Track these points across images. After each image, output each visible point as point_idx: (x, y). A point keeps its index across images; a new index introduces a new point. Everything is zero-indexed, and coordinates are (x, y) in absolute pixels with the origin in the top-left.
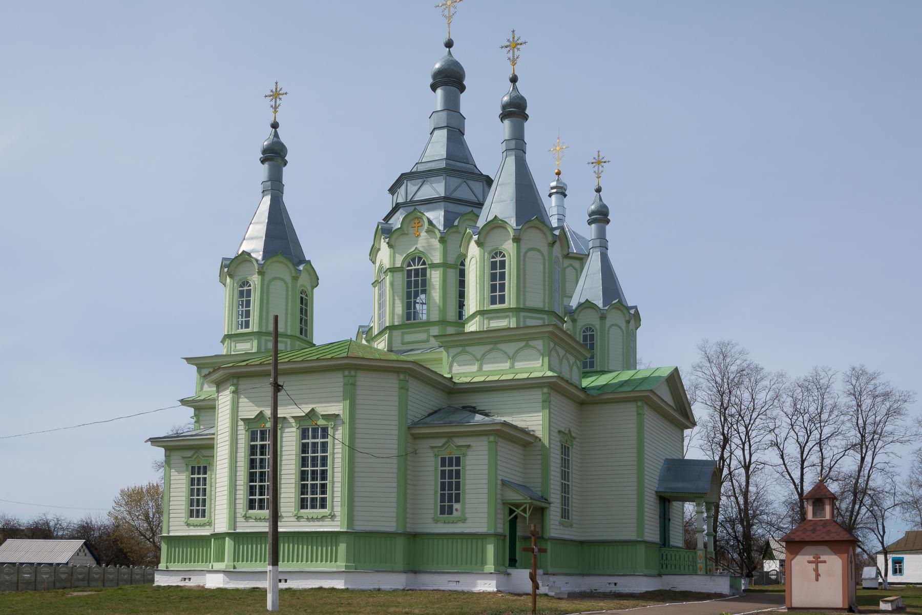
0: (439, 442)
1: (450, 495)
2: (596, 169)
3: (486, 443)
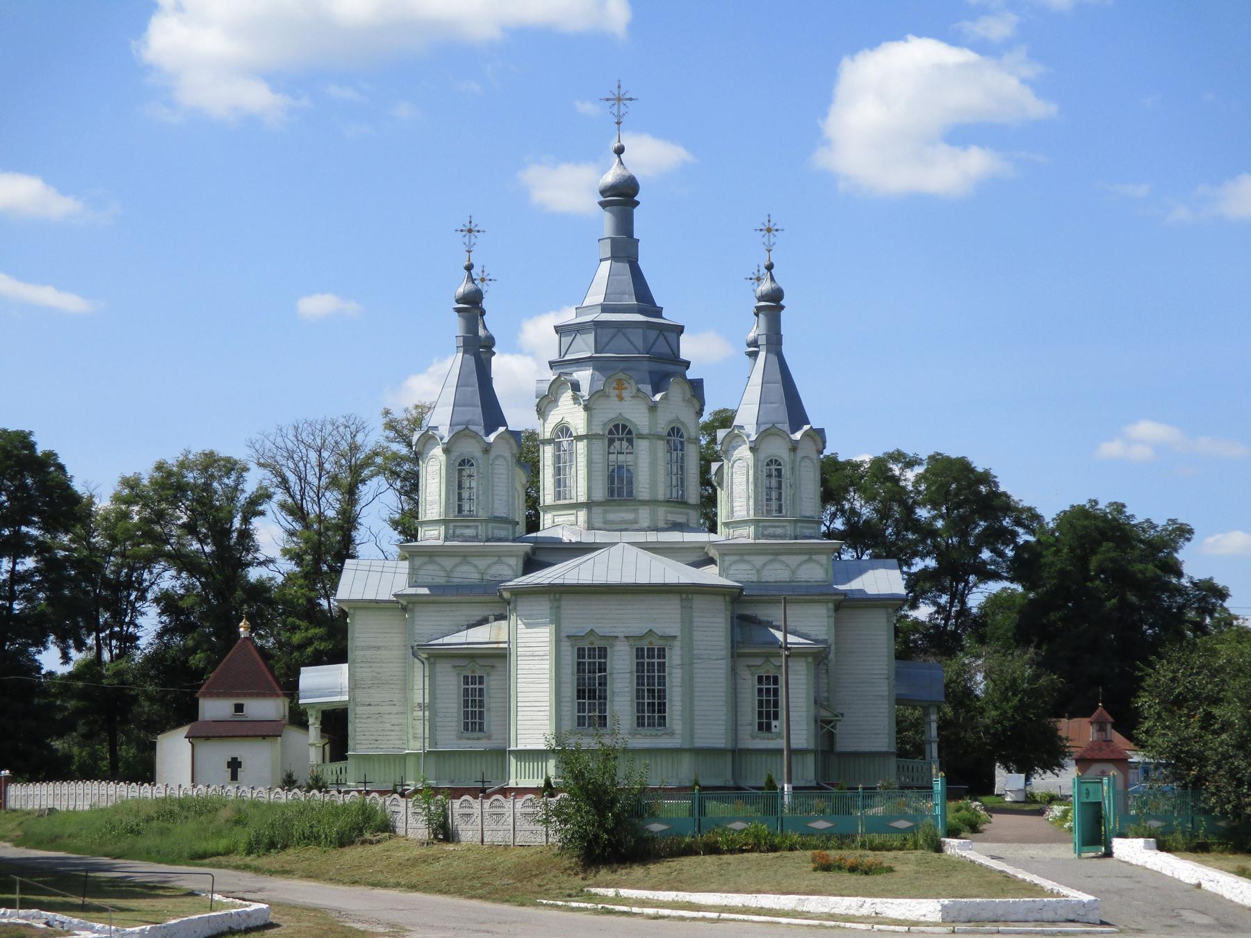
0: (759, 661)
1: (768, 713)
2: (615, 110)
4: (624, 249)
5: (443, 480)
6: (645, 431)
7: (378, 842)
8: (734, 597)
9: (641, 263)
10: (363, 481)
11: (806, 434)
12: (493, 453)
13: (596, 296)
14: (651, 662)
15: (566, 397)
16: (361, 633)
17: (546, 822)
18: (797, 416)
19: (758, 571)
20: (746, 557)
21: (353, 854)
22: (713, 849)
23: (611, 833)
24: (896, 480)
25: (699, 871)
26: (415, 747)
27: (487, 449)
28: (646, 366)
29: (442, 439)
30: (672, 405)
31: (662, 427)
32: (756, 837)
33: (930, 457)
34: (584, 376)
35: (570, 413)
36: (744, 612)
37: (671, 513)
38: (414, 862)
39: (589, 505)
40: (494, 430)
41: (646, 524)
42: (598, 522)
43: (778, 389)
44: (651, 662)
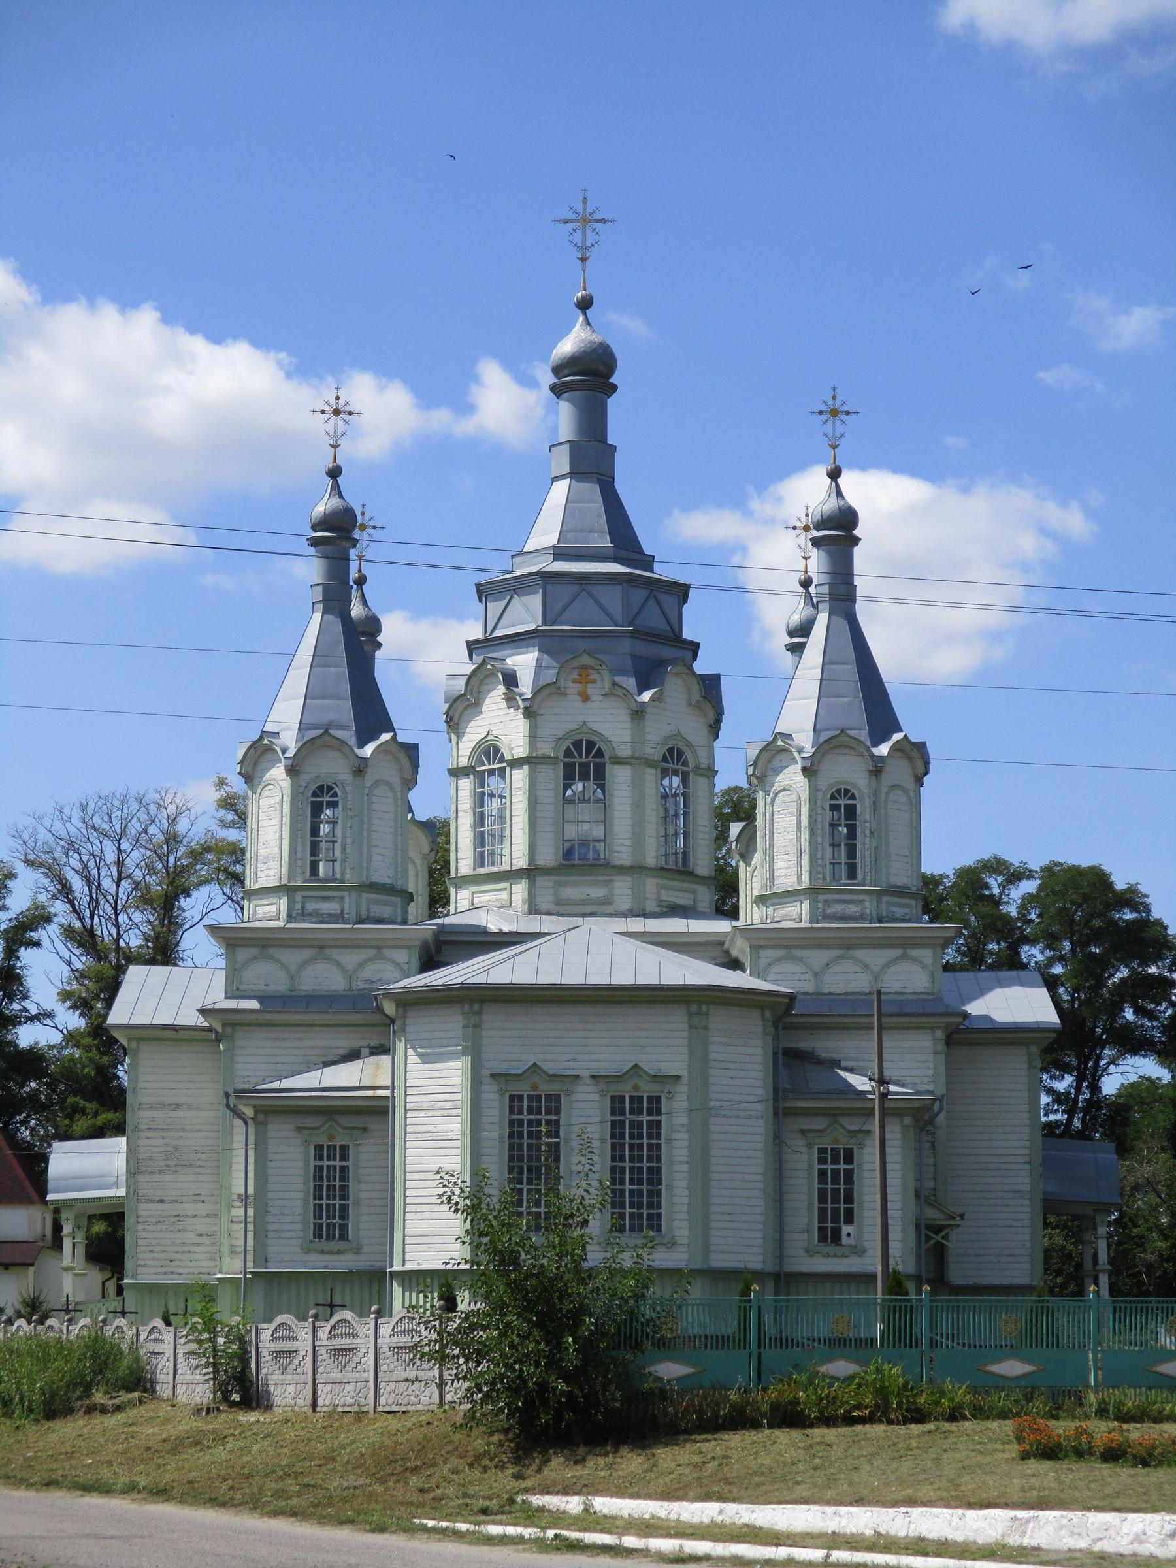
0: (820, 1123)
1: (836, 1211)
2: (578, 238)
4: (592, 459)
5: (287, 820)
6: (625, 751)
7: (118, 1408)
8: (779, 1011)
9: (619, 485)
10: (187, 893)
11: (896, 748)
12: (370, 778)
13: (546, 532)
14: (635, 1118)
15: (496, 696)
16: (143, 1078)
17: (442, 1358)
18: (882, 718)
19: (816, 975)
20: (798, 953)
21: (65, 1431)
22: (789, 1417)
23: (574, 1377)
24: (995, 902)
25: (766, 1460)
26: (232, 1268)
27: (360, 768)
28: (627, 646)
29: (284, 751)
30: (670, 712)
31: (654, 751)
32: (882, 1392)
33: (1043, 869)
34: (524, 663)
35: (501, 723)
36: (795, 1038)
37: (667, 888)
38: (176, 1446)
39: (530, 873)
40: (375, 737)
41: (626, 906)
42: (545, 902)
43: (850, 671)
44: (635, 1118)
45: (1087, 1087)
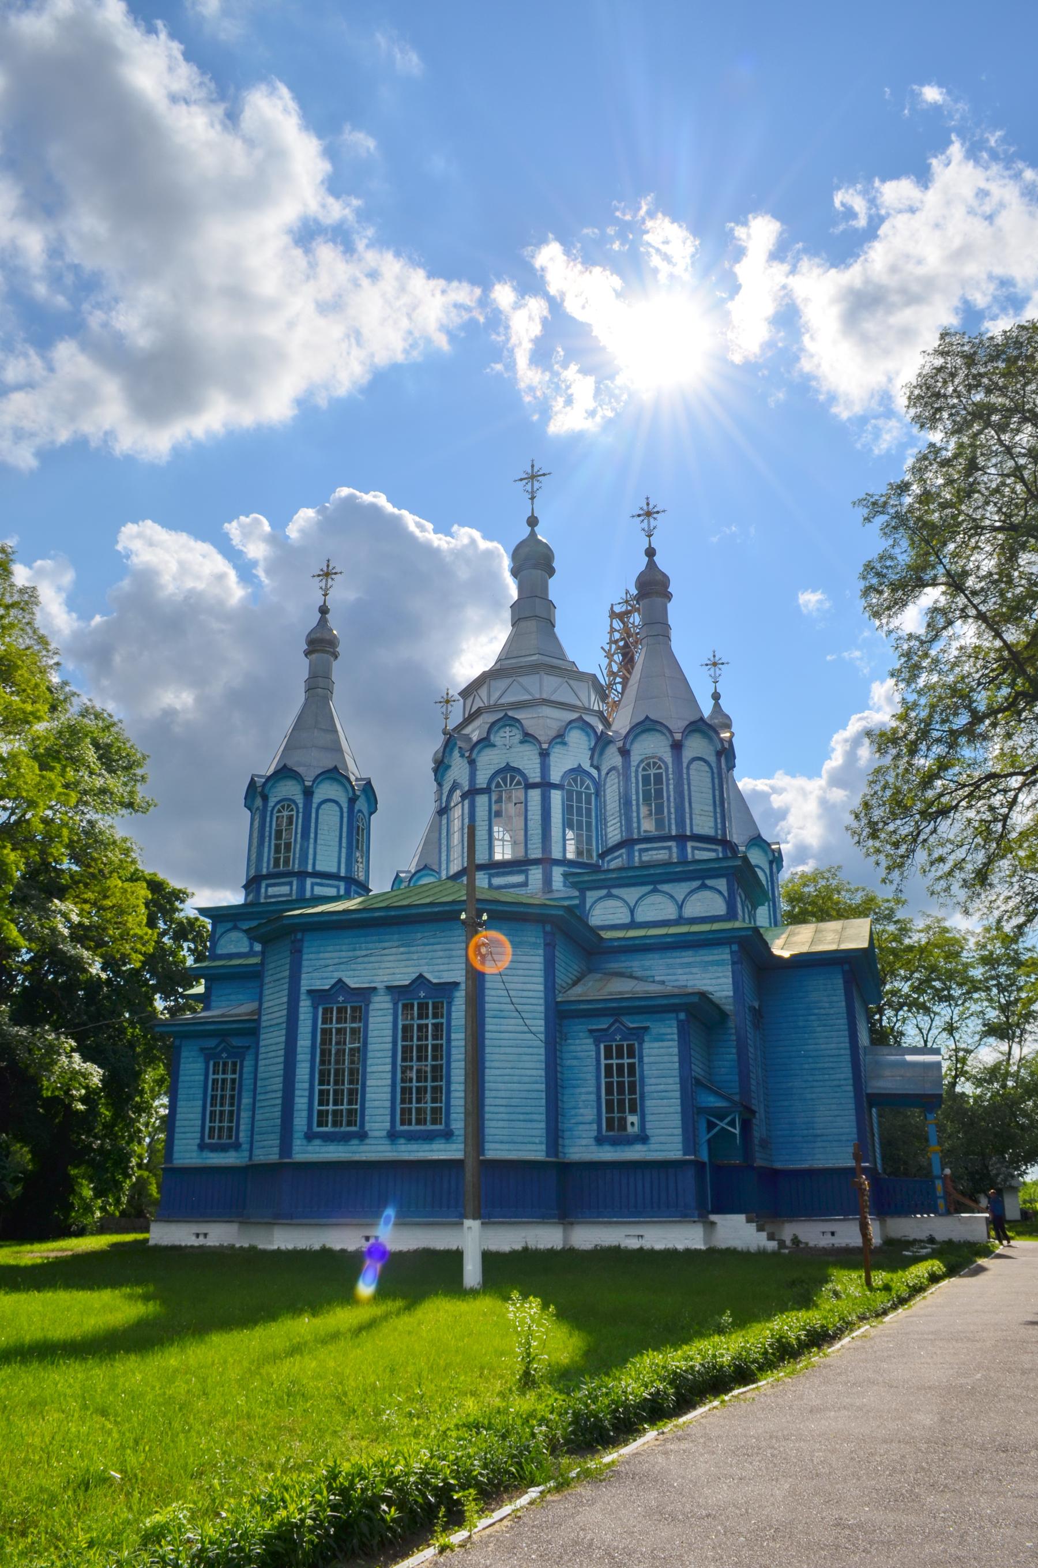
2: (712, 671)
3: (674, 1023)
45: (932, 788)
